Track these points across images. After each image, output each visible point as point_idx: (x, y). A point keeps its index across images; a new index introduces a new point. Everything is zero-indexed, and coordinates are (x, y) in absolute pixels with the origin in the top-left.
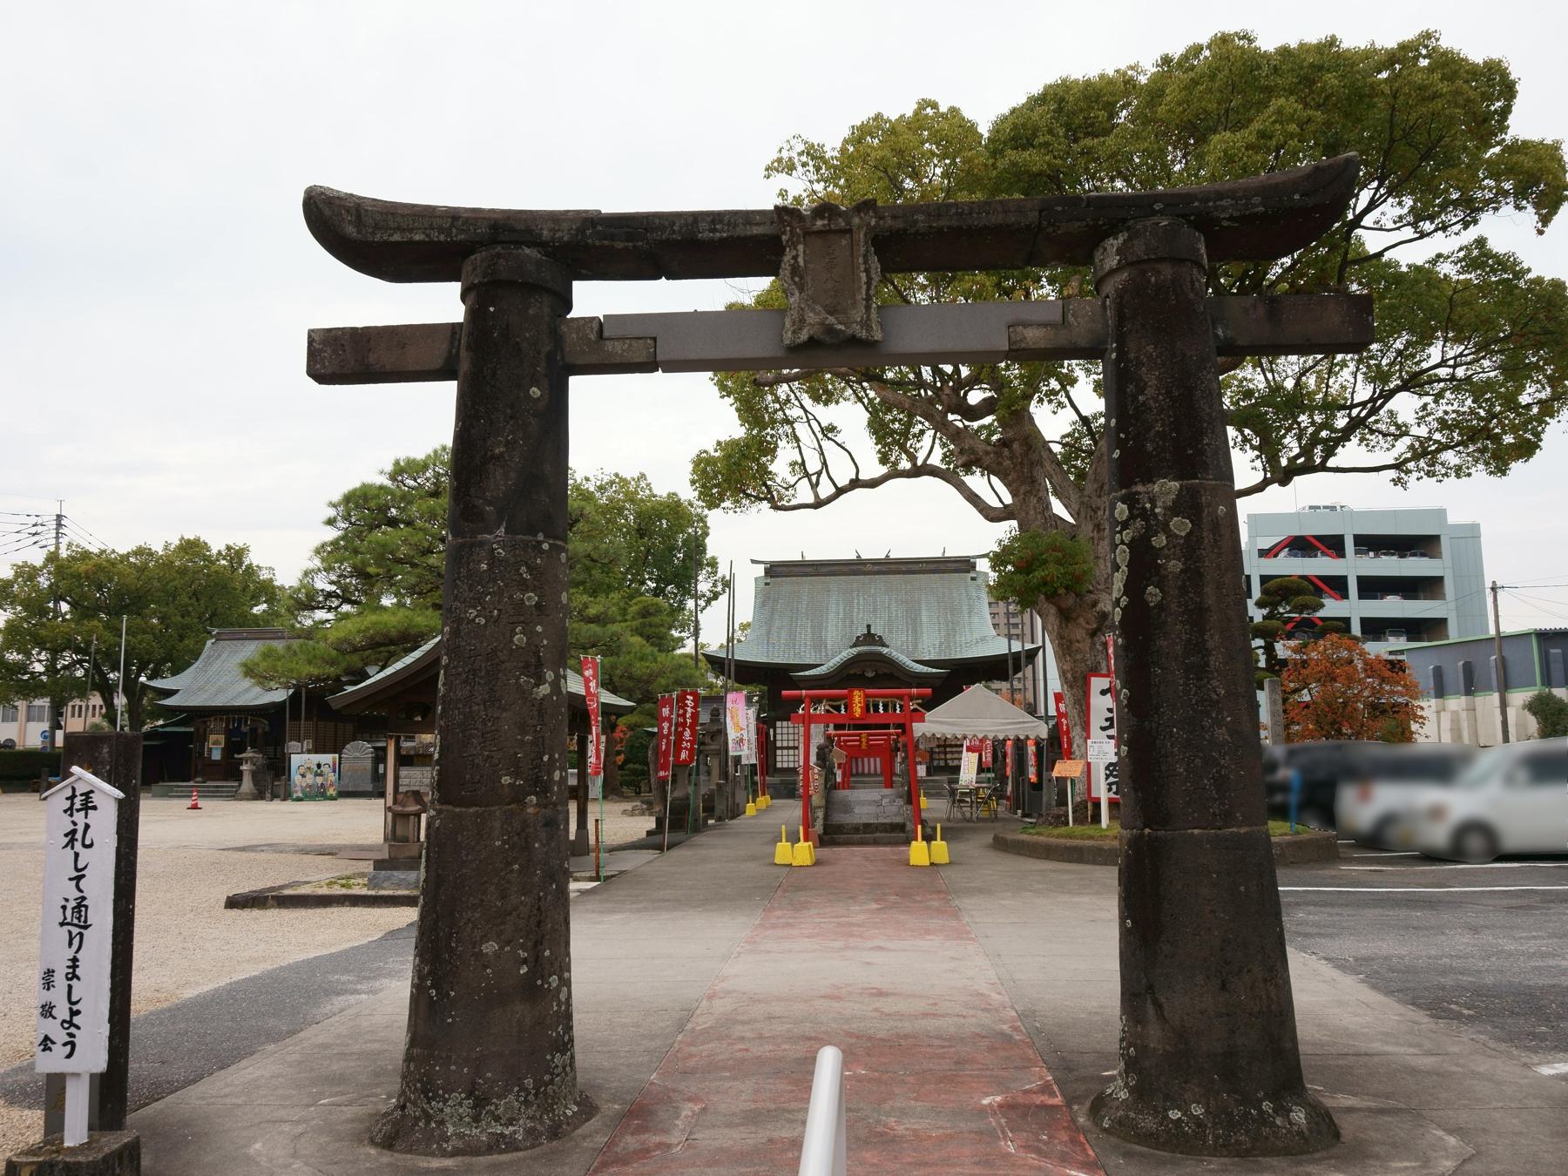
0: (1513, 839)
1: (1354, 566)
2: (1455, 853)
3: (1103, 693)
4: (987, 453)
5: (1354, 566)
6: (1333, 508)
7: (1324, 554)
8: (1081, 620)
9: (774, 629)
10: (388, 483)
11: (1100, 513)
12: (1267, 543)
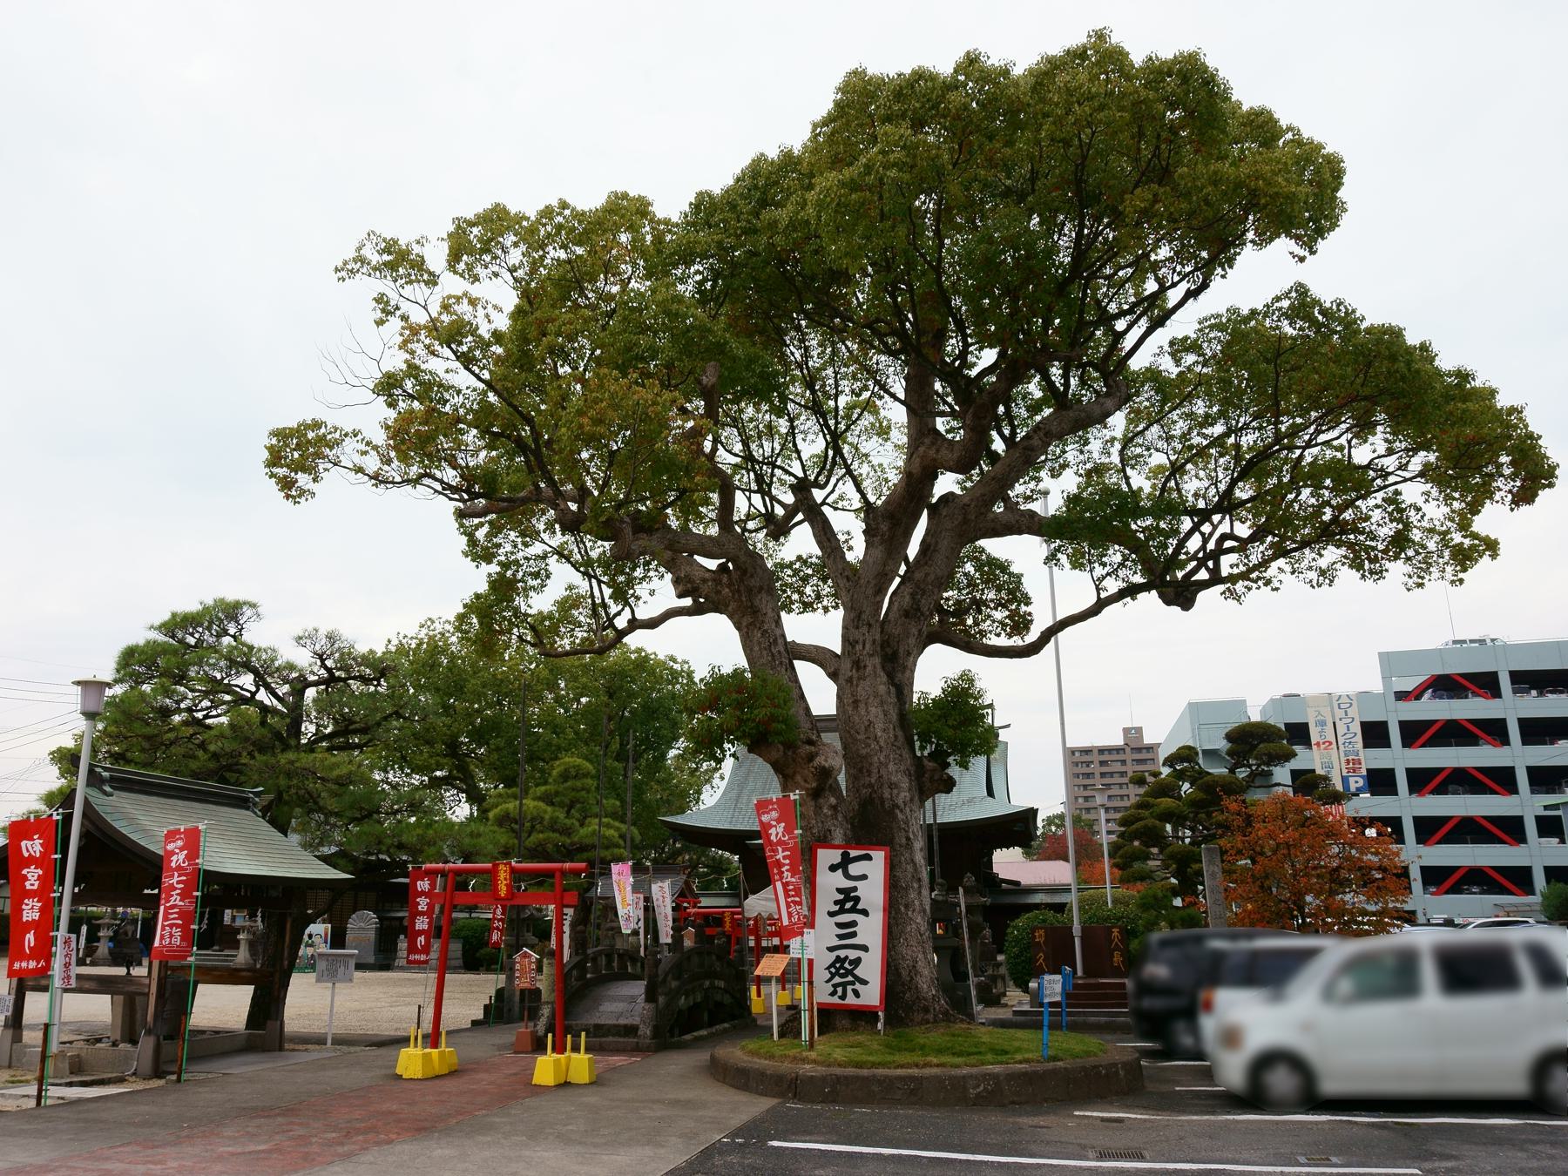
0: (1330, 1086)
1: (1513, 707)
2: (1253, 1098)
3: (833, 868)
4: (704, 581)
5: (1513, 707)
6: (1482, 642)
7: (1475, 694)
8: (798, 778)
9: (746, 792)
10: (161, 638)
11: (859, 647)
12: (1409, 685)
